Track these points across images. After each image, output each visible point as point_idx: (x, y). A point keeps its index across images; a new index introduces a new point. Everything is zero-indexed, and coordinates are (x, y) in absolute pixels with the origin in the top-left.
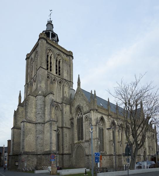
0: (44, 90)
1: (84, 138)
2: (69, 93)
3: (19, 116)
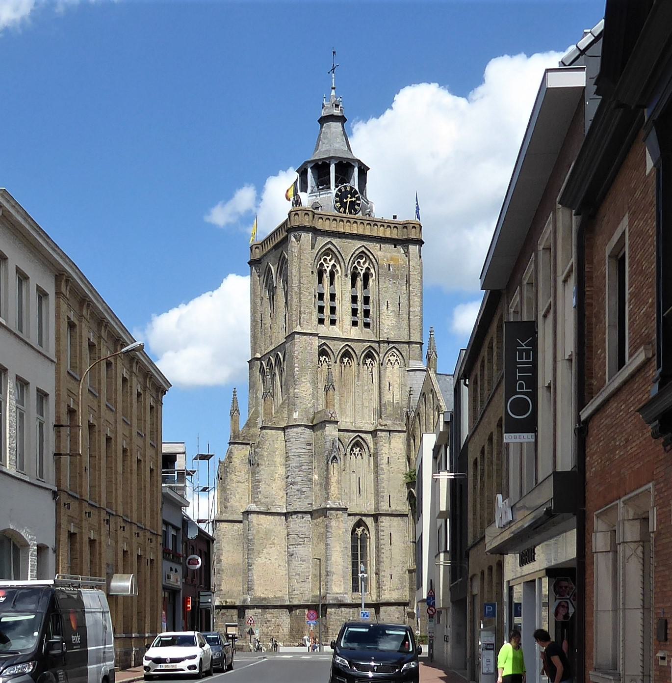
0: (309, 405)
2: (402, 386)
3: (234, 477)
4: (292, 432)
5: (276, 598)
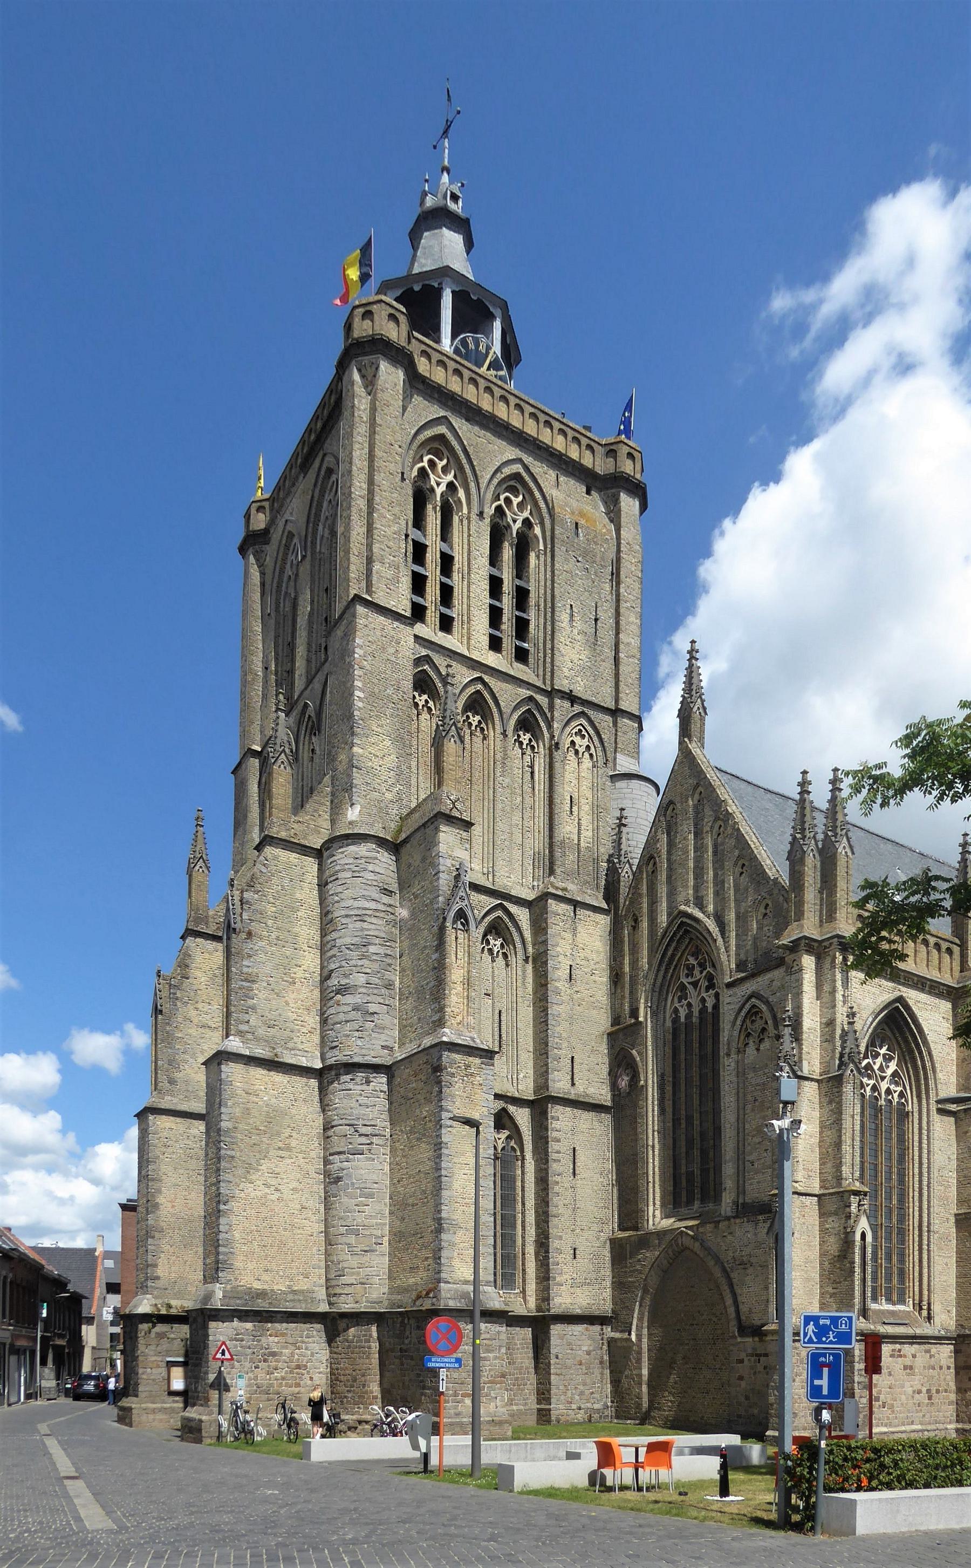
0: (389, 796)
1: (729, 1183)
2: (597, 811)
3: (192, 1013)
4: (346, 856)
5: (294, 1292)
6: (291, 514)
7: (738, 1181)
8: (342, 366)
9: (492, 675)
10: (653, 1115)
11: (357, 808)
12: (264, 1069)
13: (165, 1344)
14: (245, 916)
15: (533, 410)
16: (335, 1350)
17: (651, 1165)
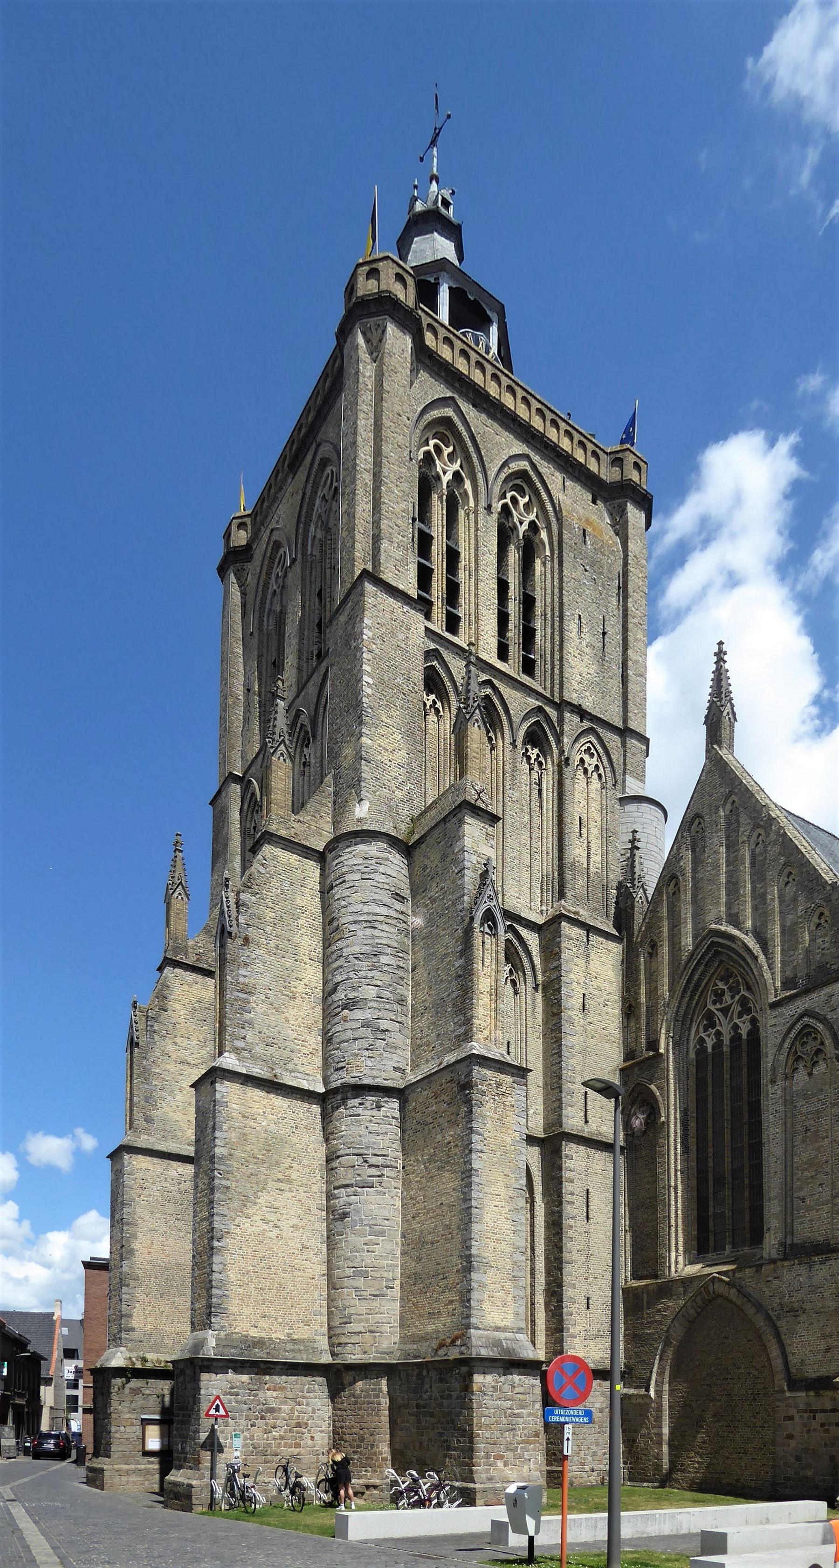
0: (399, 794)
2: (607, 835)
3: (171, 1048)
5: (294, 1341)
6: (278, 522)
7: (786, 1219)
8: (344, 333)
9: (501, 680)
10: (676, 1154)
11: (366, 805)
12: (262, 1090)
13: (139, 1401)
14: (242, 920)
15: (539, 406)
16: (340, 1406)
17: (673, 1208)
